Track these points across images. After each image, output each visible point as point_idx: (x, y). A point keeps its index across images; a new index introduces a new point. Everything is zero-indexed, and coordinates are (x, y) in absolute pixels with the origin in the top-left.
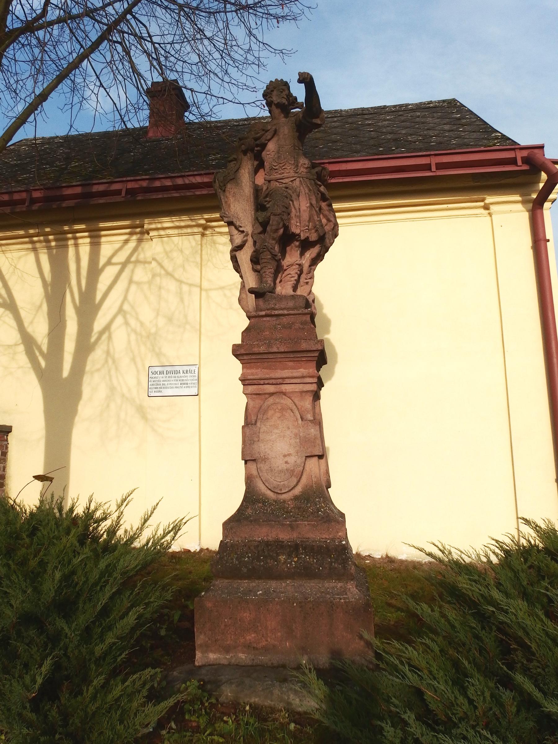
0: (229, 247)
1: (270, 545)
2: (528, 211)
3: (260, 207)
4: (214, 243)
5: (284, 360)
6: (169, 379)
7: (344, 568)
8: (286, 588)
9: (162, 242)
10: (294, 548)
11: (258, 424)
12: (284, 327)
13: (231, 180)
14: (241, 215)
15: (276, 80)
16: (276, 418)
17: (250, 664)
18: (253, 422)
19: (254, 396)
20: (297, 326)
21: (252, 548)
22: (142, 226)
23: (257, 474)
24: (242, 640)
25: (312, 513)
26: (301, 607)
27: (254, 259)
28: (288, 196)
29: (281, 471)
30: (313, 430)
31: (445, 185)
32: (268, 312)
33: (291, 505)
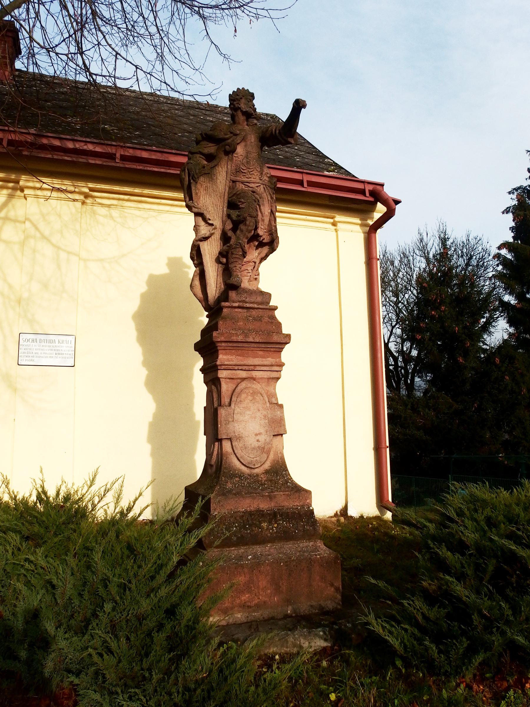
0: (192, 236)
1: (253, 514)
2: (364, 233)
3: (232, 205)
4: (94, 213)
5: (256, 349)
6: (43, 348)
7: (315, 529)
8: (269, 550)
9: (38, 202)
10: (273, 516)
11: (233, 405)
12: (255, 319)
13: (206, 174)
14: (210, 208)
15: (243, 88)
16: (249, 401)
17: (245, 621)
18: (227, 403)
19: (228, 380)
20: (266, 319)
21: (238, 518)
22: (17, 182)
23: (232, 451)
24: (238, 601)
25: (282, 484)
26: (287, 566)
27: (225, 253)
28: (257, 200)
29: (254, 449)
30: (279, 412)
31: (294, 198)
32: (241, 304)
33: (263, 478)
